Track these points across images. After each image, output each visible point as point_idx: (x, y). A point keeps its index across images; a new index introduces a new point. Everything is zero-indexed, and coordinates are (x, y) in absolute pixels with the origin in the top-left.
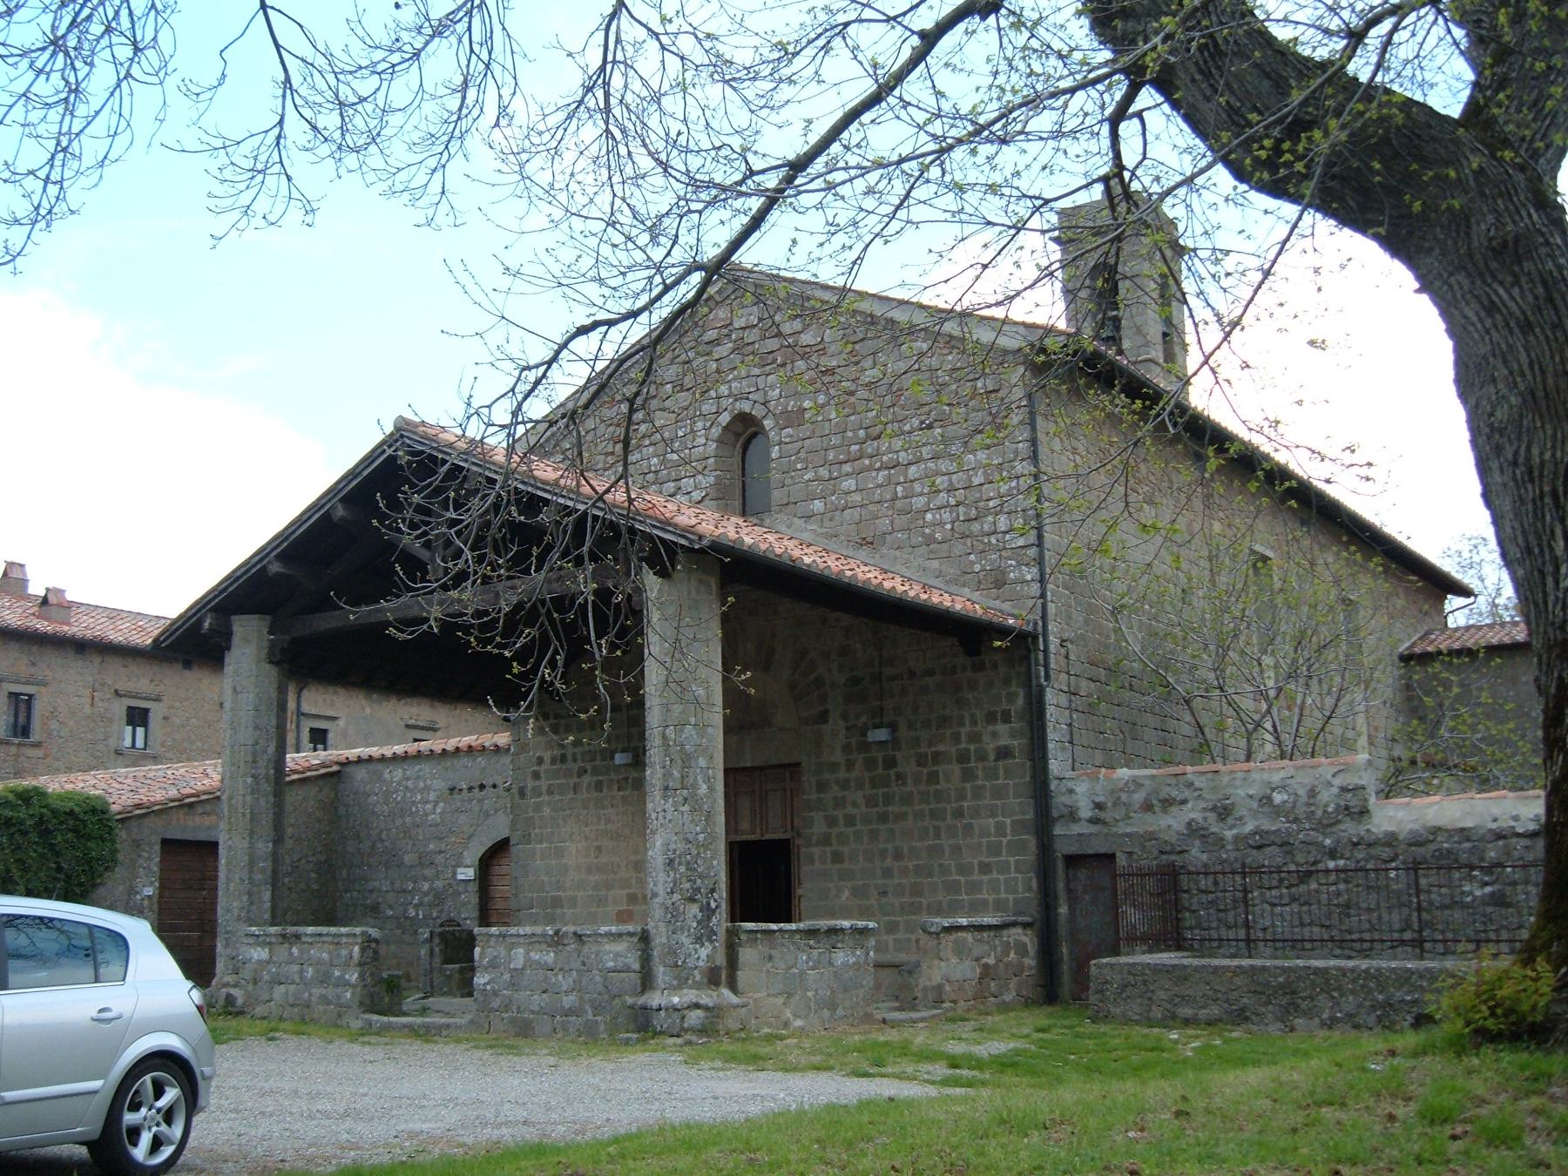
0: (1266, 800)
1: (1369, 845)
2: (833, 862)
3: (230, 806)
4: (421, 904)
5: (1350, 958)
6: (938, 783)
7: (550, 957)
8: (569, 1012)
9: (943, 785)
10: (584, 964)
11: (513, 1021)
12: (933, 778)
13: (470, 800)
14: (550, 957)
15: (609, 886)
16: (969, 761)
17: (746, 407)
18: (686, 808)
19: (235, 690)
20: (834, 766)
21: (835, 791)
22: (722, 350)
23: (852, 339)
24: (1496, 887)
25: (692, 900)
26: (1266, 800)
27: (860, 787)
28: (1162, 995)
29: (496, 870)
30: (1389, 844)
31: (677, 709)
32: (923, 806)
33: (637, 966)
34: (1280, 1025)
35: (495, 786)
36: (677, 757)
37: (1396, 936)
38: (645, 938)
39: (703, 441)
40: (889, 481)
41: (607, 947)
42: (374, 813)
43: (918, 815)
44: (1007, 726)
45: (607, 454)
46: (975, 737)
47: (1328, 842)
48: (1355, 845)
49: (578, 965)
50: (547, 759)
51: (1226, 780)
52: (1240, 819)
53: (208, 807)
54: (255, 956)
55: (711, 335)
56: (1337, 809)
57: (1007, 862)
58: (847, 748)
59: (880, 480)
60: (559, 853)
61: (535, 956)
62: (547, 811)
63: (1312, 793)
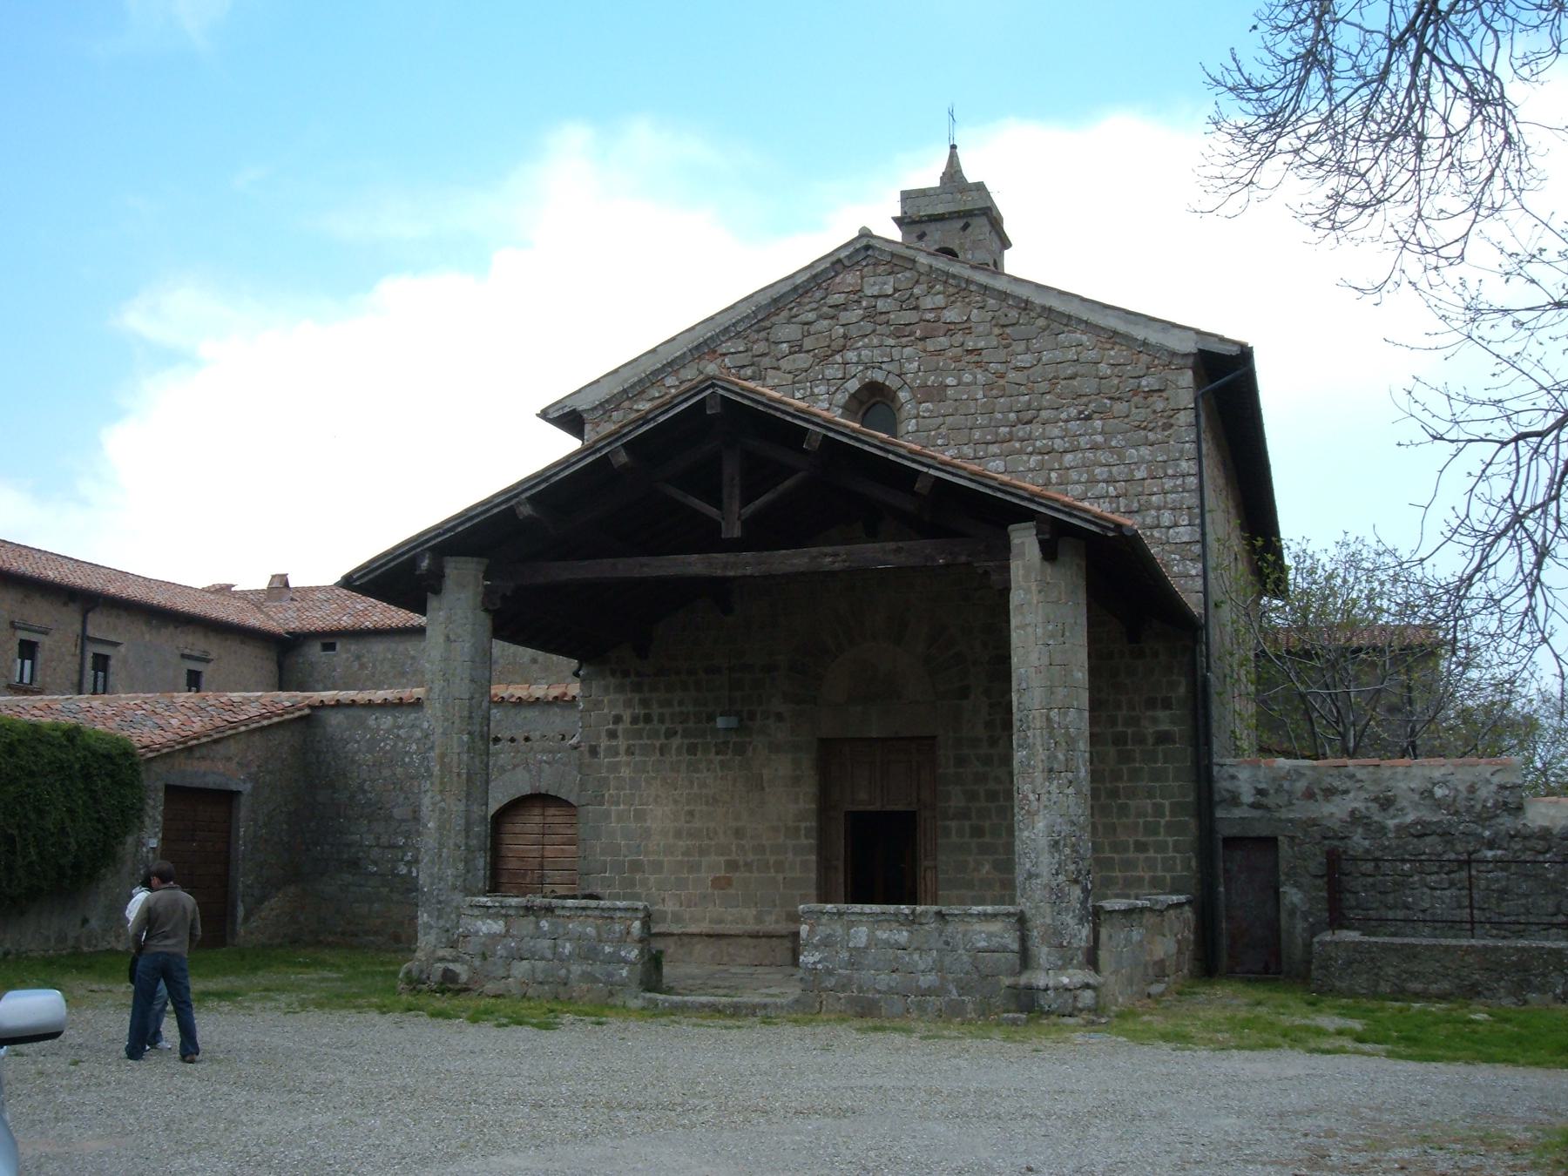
0: (1427, 794)
1: (1525, 838)
2: (972, 836)
3: (443, 765)
5: (1504, 938)
7: (903, 936)
8: (928, 992)
11: (852, 1001)
15: (703, 852)
16: (1125, 743)
17: (879, 376)
18: (1071, 790)
19: (448, 638)
22: (855, 314)
23: (1003, 321)
25: (1076, 881)
26: (1427, 794)
28: (1390, 971)
29: (508, 827)
31: (1061, 692)
33: (1015, 946)
35: (512, 740)
36: (1062, 740)
37: (1546, 919)
38: (1022, 920)
40: (1042, 466)
41: (977, 927)
42: (353, 761)
47: (1487, 833)
48: (1512, 837)
49: (940, 945)
50: (627, 716)
51: (1388, 773)
52: (1402, 809)
53: (204, 751)
54: (484, 929)
55: (838, 298)
56: (1495, 805)
59: (1032, 464)
60: (640, 816)
61: (882, 935)
62: (625, 772)
63: (1472, 789)
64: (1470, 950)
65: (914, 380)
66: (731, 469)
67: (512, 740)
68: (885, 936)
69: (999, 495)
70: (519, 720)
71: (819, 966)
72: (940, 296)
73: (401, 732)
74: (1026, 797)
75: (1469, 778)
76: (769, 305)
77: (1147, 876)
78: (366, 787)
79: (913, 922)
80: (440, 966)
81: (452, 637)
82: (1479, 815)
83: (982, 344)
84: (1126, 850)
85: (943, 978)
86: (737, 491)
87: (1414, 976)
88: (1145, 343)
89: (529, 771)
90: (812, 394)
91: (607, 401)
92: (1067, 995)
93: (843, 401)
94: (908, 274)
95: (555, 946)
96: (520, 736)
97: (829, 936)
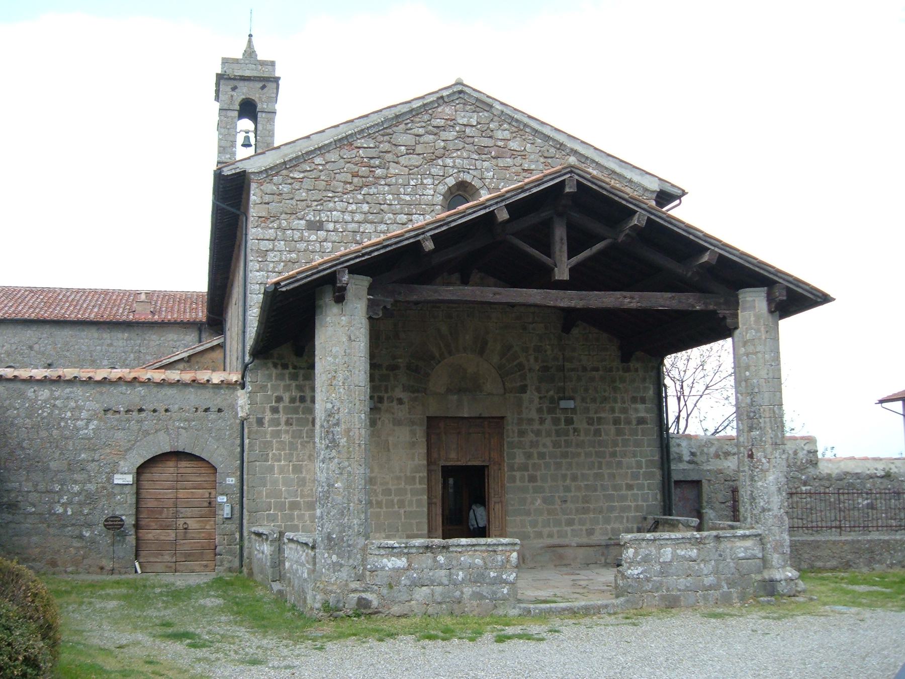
2: (529, 481)
4: (70, 503)
6: (600, 436)
7: (694, 553)
8: (710, 588)
9: (604, 437)
10: (721, 555)
11: (662, 598)
12: (597, 433)
13: (128, 420)
14: (694, 553)
16: (620, 424)
17: (468, 178)
20: (530, 421)
21: (531, 436)
23: (546, 154)
24: (869, 501)
27: (549, 434)
28: (806, 556)
30: (828, 480)
32: (591, 449)
34: (867, 568)
39: (432, 192)
42: (12, 424)
43: (588, 455)
44: (644, 406)
45: (346, 183)
46: (624, 410)
49: (716, 557)
54: (390, 565)
57: (643, 484)
58: (540, 410)
61: (681, 552)
63: (795, 453)
64: (845, 542)
65: (490, 183)
66: (560, 233)
67: (155, 411)
68: (683, 553)
69: (757, 269)
70: (160, 395)
71: (641, 576)
72: (507, 132)
73: (57, 402)
74: (759, 461)
75: (794, 447)
76: (392, 119)
77: (633, 504)
78: (25, 445)
79: (700, 543)
80: (355, 596)
81: (353, 338)
82: (799, 467)
83: (533, 167)
84: (620, 489)
85: (718, 578)
86: (565, 248)
87: (819, 558)
88: (630, 181)
89: (169, 434)
90: (422, 183)
91: (271, 168)
92: (792, 583)
93: (443, 191)
94: (486, 114)
95: (450, 574)
96: (161, 407)
97: (647, 555)
